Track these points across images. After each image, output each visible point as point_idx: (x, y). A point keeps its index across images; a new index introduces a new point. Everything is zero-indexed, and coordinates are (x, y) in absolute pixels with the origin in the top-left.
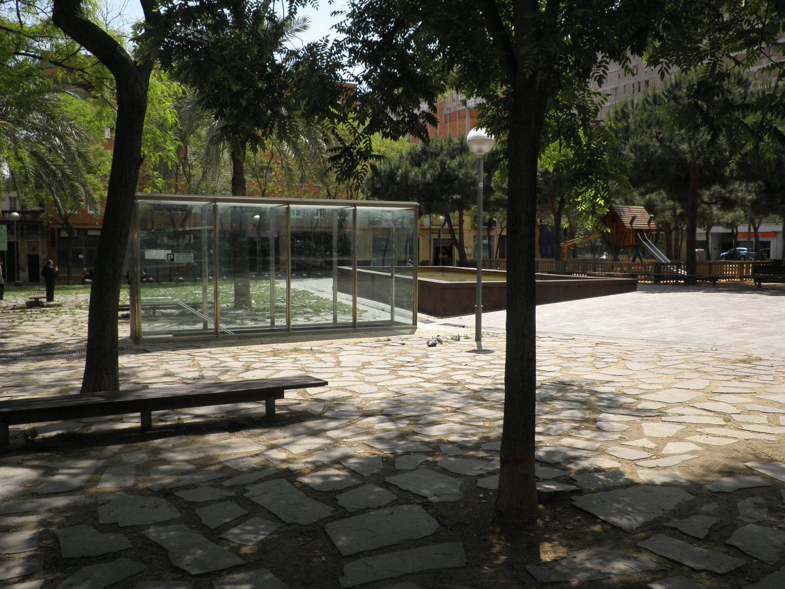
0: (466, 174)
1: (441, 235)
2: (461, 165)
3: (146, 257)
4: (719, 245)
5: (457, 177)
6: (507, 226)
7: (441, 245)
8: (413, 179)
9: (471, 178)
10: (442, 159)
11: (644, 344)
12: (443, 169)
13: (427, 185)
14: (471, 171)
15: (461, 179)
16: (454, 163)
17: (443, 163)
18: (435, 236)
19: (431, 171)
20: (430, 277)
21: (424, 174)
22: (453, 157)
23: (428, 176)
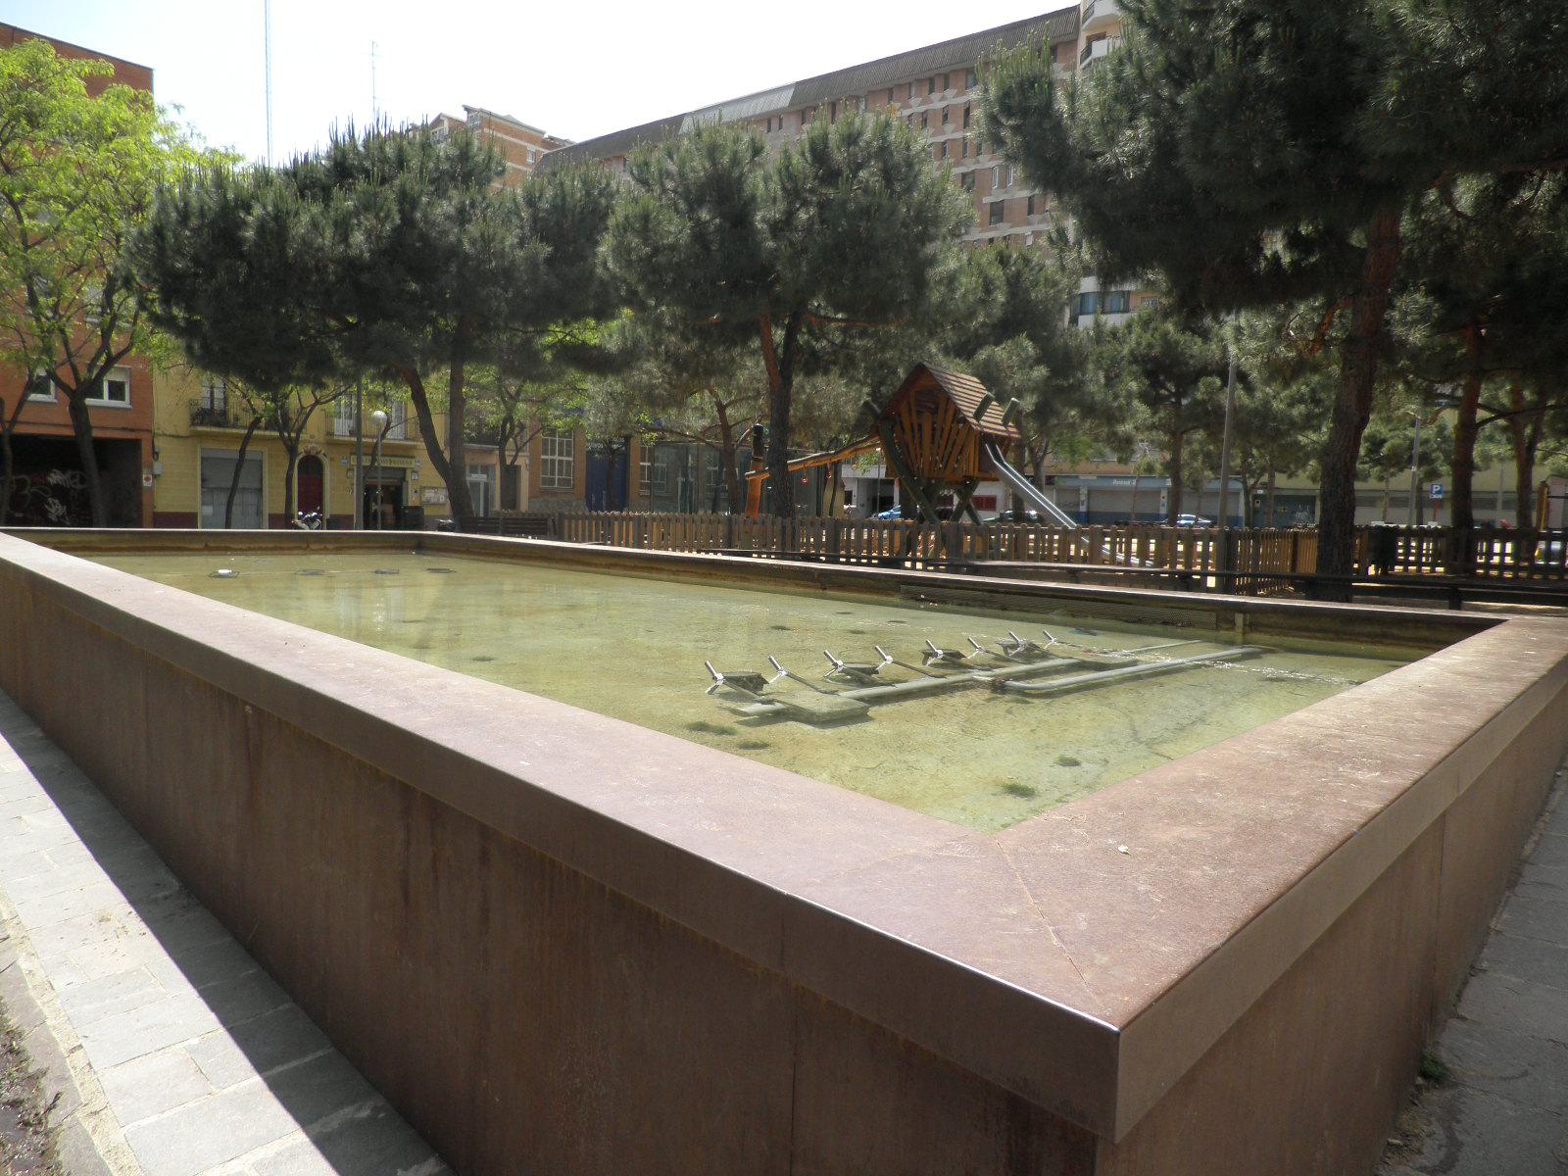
0: (486, 240)
1: (379, 458)
2: (462, 216)
3: (1209, 578)
4: (868, 500)
5: (454, 251)
6: (1135, 276)
7: (380, 482)
8: (306, 243)
9: (502, 255)
10: (403, 186)
11: (862, 704)
12: (408, 221)
13: (351, 266)
14: (501, 232)
15: (467, 257)
16: (446, 207)
17: (408, 202)
18: (366, 461)
19: (368, 221)
20: (1413, 606)
21: (343, 228)
22: (440, 193)
23: (358, 238)
